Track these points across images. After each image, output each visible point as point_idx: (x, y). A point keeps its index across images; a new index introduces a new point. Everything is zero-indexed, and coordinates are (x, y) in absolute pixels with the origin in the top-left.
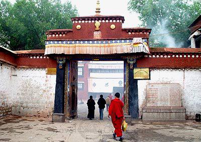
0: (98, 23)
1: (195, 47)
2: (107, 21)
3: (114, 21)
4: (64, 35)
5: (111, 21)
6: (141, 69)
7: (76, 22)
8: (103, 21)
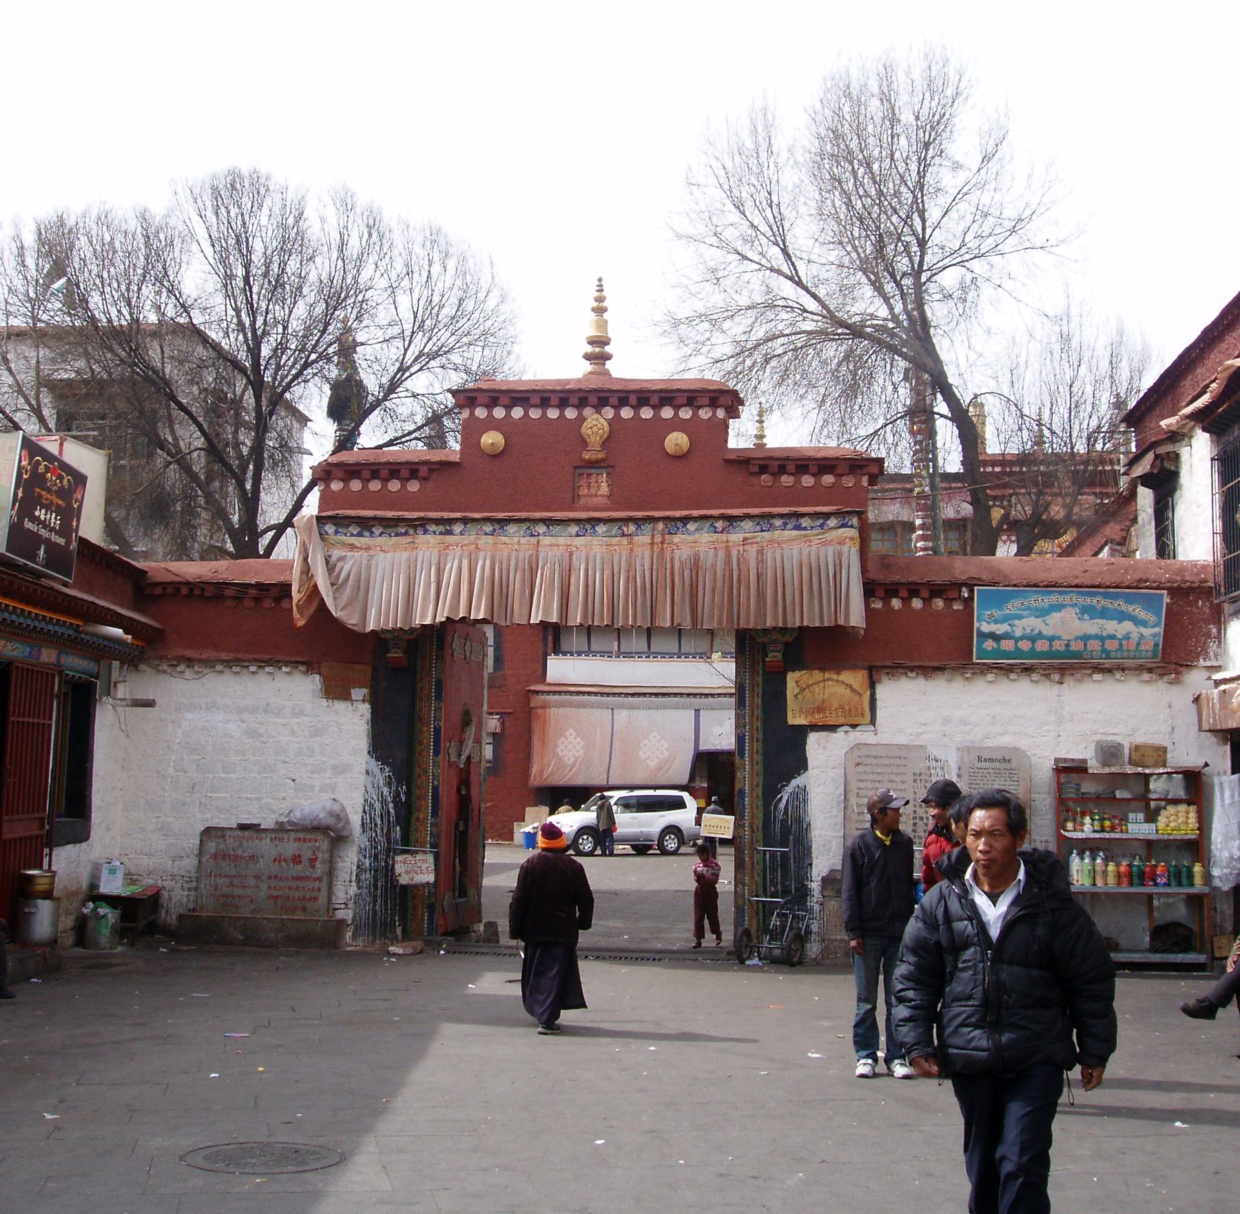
0: (596, 423)
1: (1154, 558)
2: (647, 413)
3: (686, 414)
4: (414, 486)
5: (667, 413)
6: (827, 675)
7: (481, 413)
8: (627, 413)
